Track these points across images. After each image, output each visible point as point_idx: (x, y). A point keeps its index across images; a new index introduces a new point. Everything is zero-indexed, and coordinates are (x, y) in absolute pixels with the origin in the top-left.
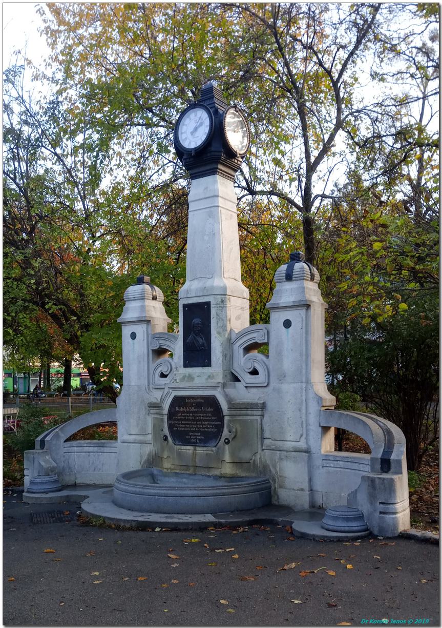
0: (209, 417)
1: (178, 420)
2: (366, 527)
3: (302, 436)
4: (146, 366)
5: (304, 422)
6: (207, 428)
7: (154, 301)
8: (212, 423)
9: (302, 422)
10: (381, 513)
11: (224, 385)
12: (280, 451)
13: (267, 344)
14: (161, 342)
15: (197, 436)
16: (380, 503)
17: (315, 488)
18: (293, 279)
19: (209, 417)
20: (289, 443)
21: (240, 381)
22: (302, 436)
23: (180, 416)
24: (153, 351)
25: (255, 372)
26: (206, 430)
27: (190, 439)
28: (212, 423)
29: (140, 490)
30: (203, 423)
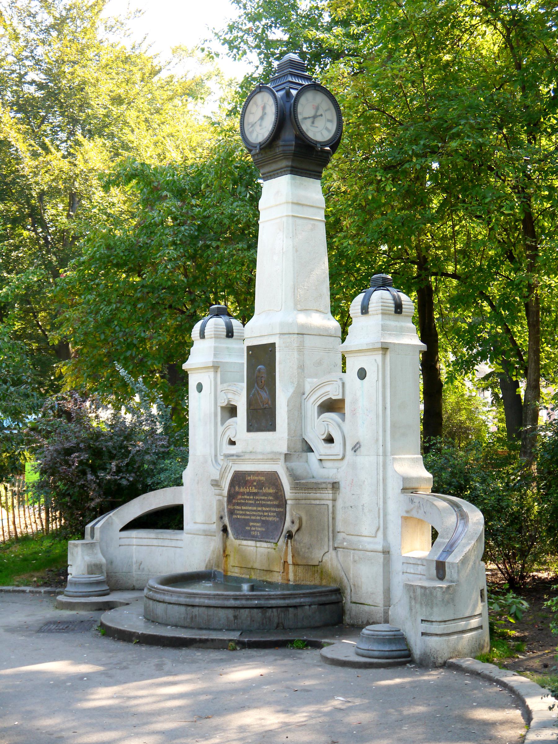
0: (270, 500)
1: (238, 504)
2: (407, 652)
3: (378, 529)
4: (213, 429)
5: (381, 511)
6: (268, 516)
7: (230, 340)
8: (274, 509)
9: (379, 510)
10: (423, 634)
11: (287, 457)
12: (354, 550)
13: (342, 401)
14: (230, 396)
15: (258, 526)
16: (422, 620)
17: (434, 623)
18: (370, 313)
19: (270, 500)
20: (365, 539)
21: (313, 451)
22: (378, 529)
23: (241, 499)
24: (222, 408)
25: (330, 440)
26: (267, 519)
27: (250, 531)
28: (274, 509)
29: (188, 600)
30: (264, 509)
